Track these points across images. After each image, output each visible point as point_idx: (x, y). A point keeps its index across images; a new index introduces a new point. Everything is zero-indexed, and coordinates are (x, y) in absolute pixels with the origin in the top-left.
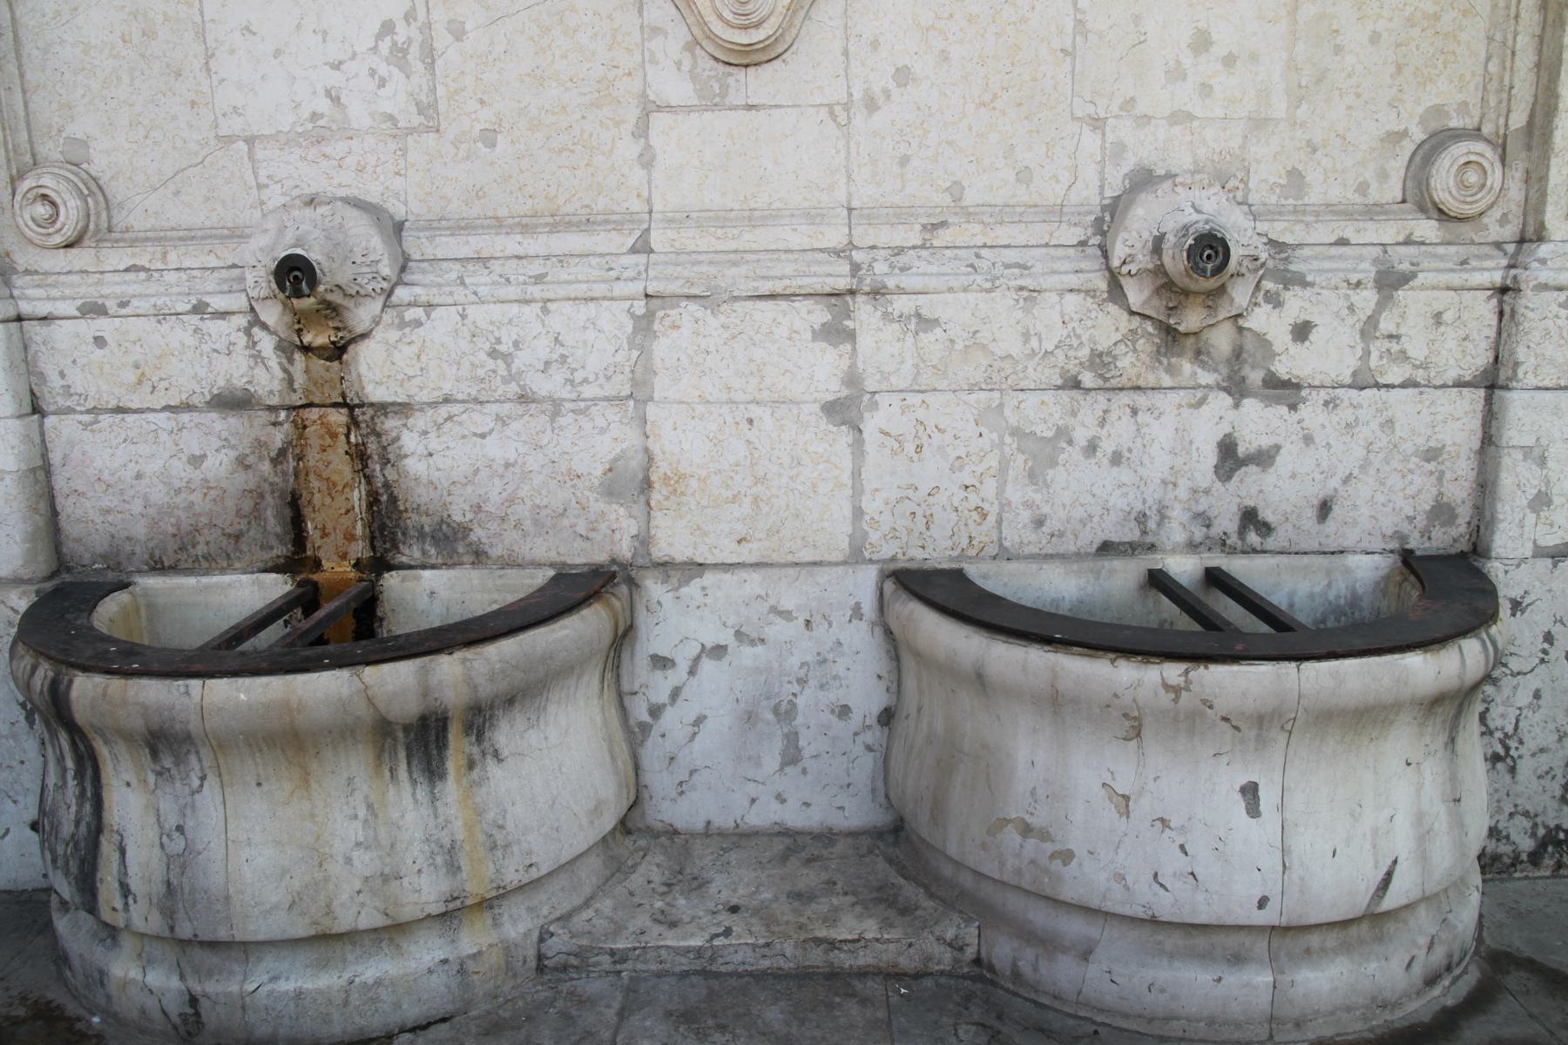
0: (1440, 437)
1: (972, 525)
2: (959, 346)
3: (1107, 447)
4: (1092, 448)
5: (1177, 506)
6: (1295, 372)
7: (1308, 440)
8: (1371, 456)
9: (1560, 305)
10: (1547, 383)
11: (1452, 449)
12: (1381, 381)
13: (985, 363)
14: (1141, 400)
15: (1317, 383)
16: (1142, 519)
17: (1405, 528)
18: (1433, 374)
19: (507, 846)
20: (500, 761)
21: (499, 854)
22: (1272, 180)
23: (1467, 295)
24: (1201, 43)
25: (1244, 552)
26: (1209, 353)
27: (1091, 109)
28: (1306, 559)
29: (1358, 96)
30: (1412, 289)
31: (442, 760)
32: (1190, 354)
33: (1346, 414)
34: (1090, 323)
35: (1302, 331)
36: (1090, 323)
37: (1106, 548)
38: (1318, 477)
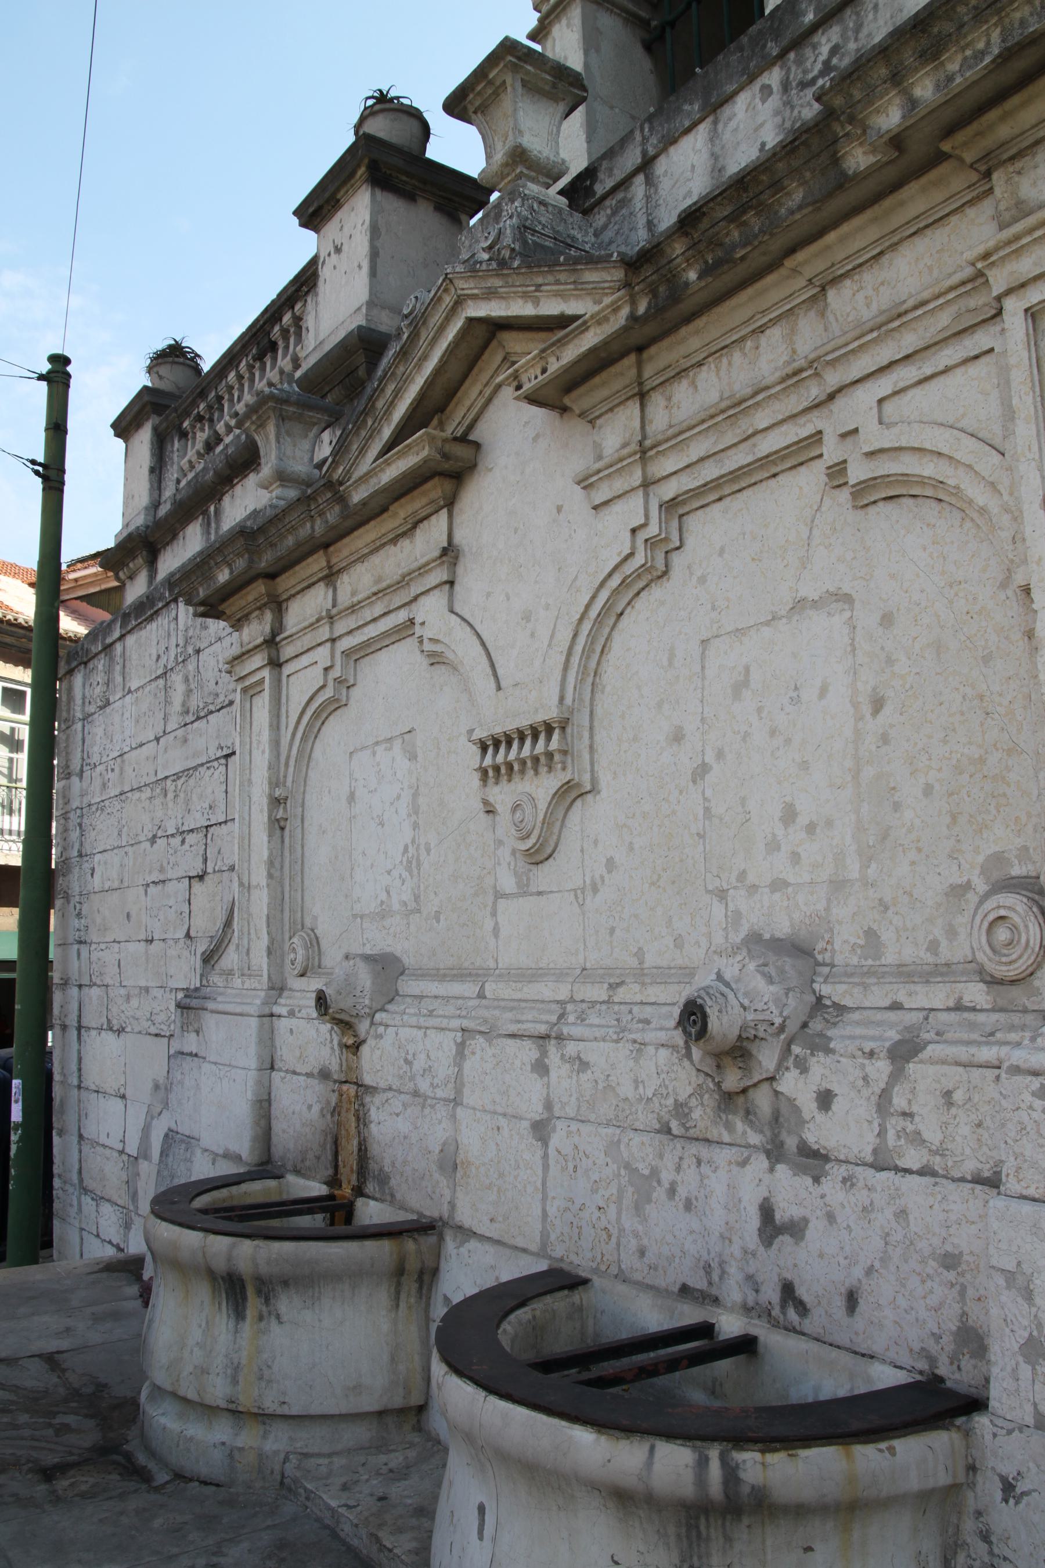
0: (956, 1241)
1: (603, 1243)
2: (600, 1087)
3: (682, 1192)
4: (672, 1191)
5: (733, 1263)
6: (822, 1142)
7: (831, 1218)
8: (890, 1248)
9: (1033, 1094)
10: (1031, 1192)
11: (971, 1259)
12: (901, 1164)
13: (615, 1103)
14: (704, 1151)
15: (842, 1157)
16: (708, 1268)
17: (934, 1348)
18: (950, 1164)
19: (269, 1381)
20: (280, 1323)
21: (263, 1384)
22: (853, 940)
23: (976, 1073)
24: (789, 815)
25: (786, 1329)
26: (755, 1114)
27: (717, 883)
28: (835, 1353)
29: (919, 850)
30: (921, 1062)
31: (244, 1308)
32: (742, 1113)
33: (862, 1196)
34: (673, 1075)
35: (825, 1099)
36: (673, 1075)
37: (685, 1290)
38: (843, 1262)
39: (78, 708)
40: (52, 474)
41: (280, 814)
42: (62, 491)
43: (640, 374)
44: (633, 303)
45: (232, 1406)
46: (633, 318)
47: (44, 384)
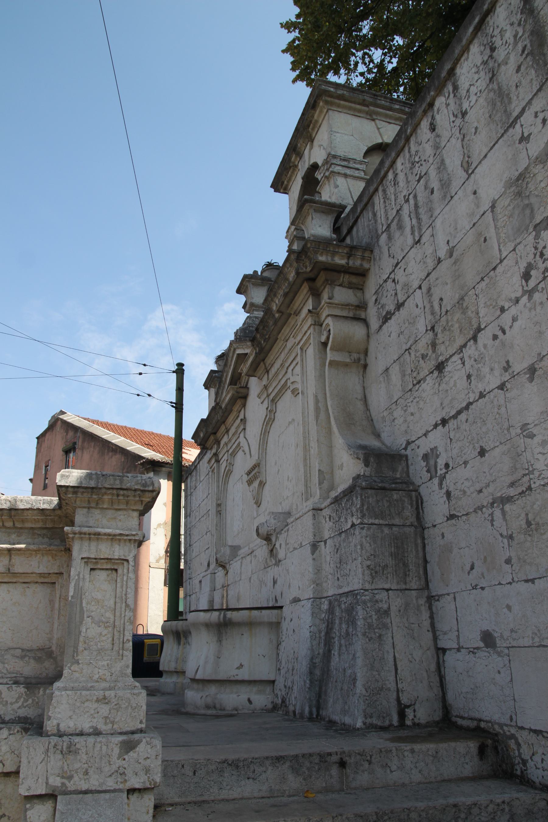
39: (189, 491)
40: (178, 406)
41: (219, 509)
42: (182, 412)
43: (265, 366)
44: (256, 350)
45: (176, 670)
46: (256, 353)
47: (175, 374)
